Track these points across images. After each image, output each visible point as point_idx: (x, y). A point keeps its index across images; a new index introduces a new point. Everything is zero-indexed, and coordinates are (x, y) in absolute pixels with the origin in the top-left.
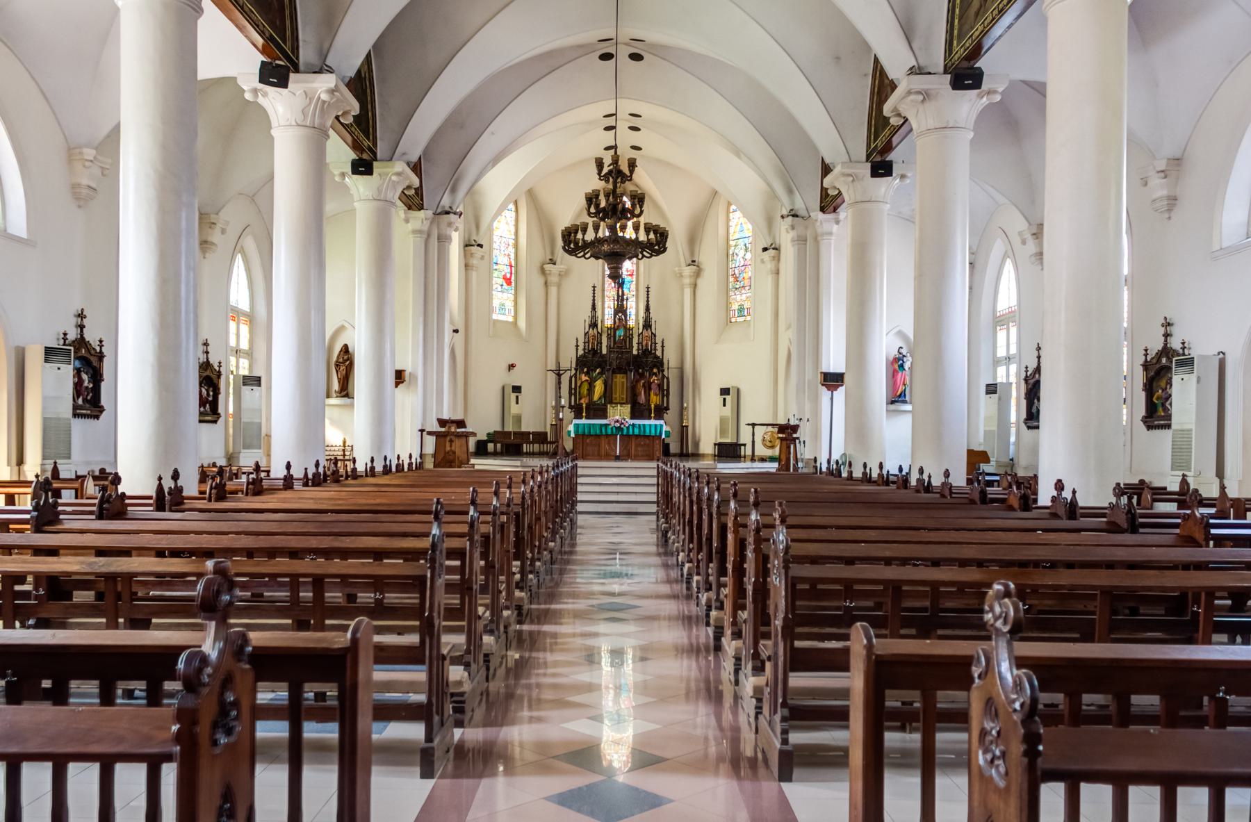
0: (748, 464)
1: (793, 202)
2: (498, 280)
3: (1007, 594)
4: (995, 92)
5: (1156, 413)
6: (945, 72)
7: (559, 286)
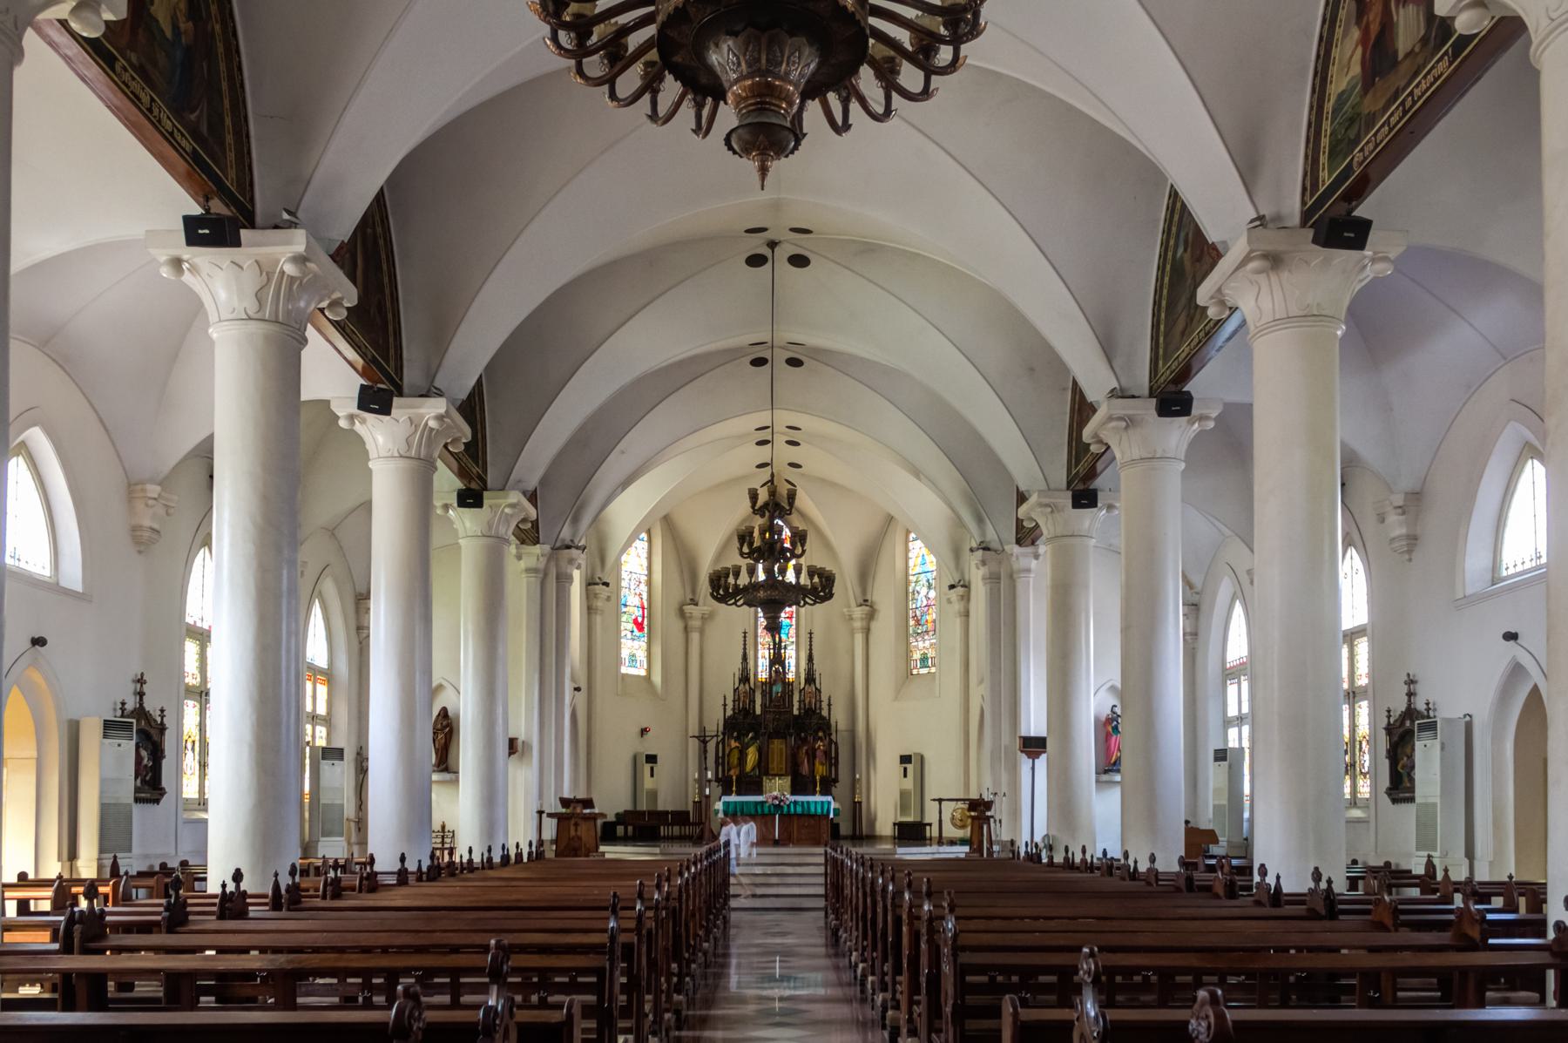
0: (935, 848)
1: (983, 533)
2: (627, 625)
3: (1092, 954)
4: (1207, 418)
5: (1400, 785)
6: (1151, 395)
7: (702, 632)
